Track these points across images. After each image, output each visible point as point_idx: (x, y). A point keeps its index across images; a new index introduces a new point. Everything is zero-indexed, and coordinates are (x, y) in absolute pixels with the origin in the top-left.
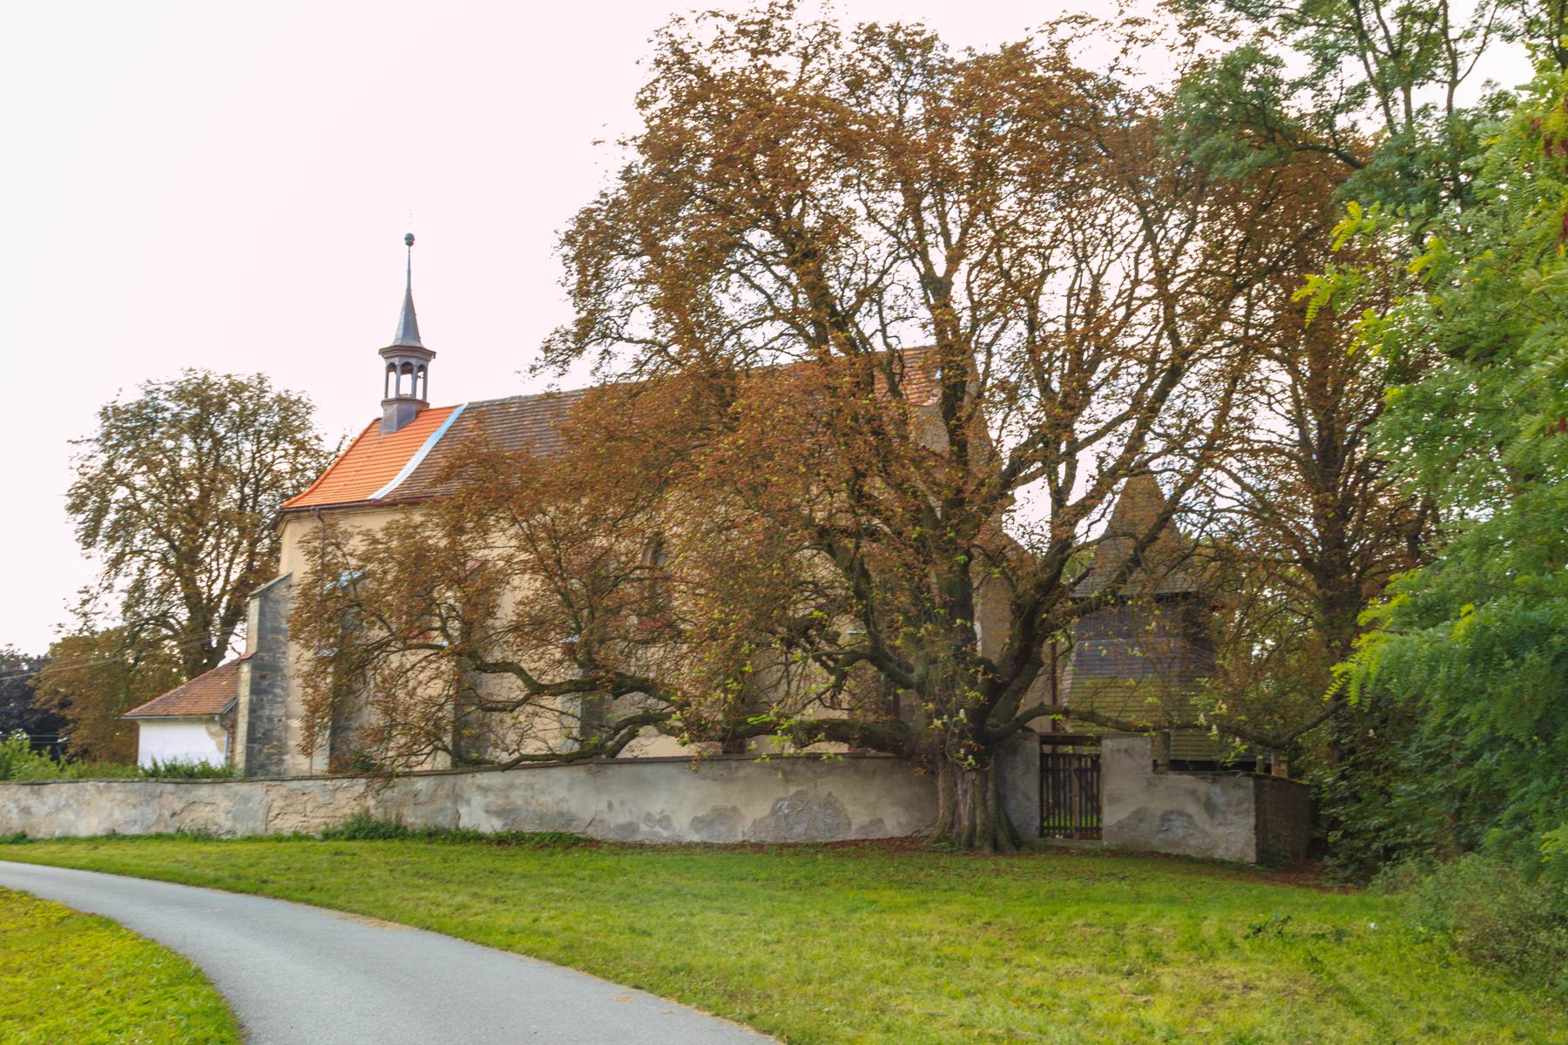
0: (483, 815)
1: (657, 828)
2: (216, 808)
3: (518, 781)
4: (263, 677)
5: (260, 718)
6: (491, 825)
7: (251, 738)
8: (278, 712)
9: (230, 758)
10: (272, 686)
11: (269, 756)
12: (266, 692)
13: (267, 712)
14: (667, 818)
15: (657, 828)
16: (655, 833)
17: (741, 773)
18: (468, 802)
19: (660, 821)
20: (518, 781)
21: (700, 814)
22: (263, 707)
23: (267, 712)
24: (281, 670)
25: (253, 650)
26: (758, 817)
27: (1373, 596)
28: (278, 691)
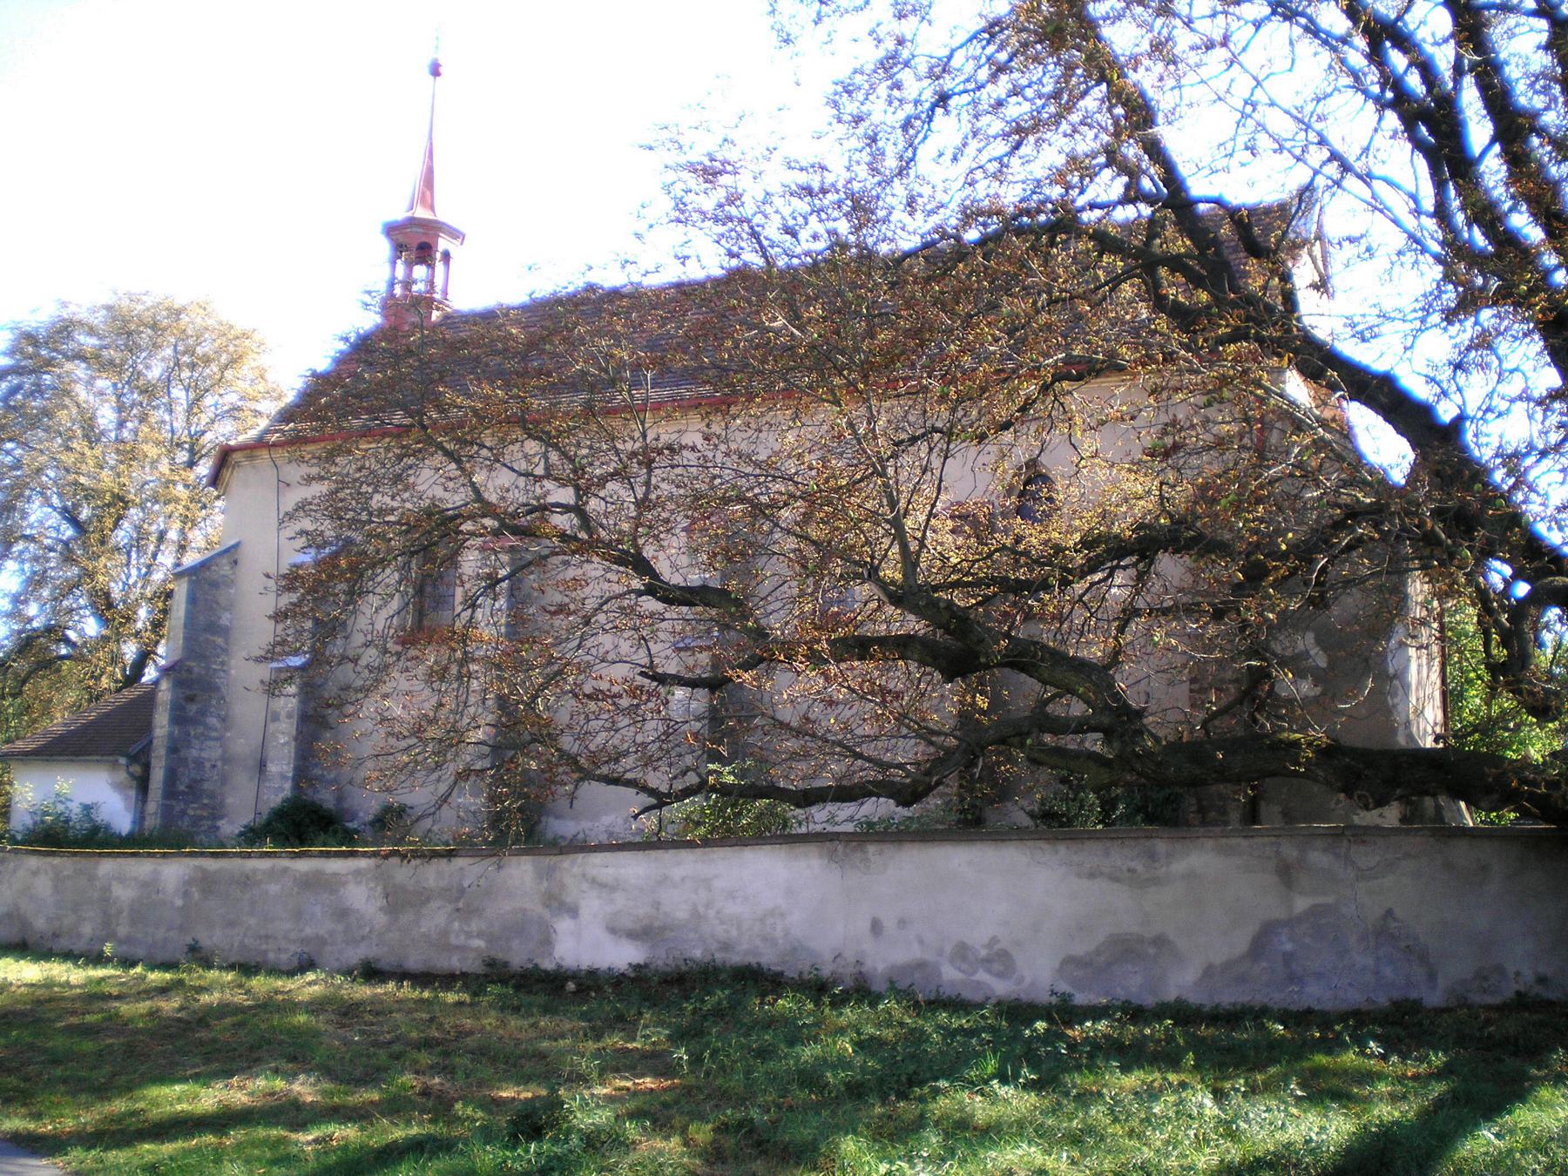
0: (606, 938)
1: (982, 976)
2: (124, 878)
3: (677, 873)
4: (191, 699)
5: (183, 761)
6: (621, 956)
7: (170, 792)
8: (212, 752)
9: (140, 817)
10: (203, 713)
11: (197, 820)
12: (194, 721)
13: (195, 753)
14: (1004, 956)
15: (982, 976)
16: (60, 798)
17: (1179, 866)
18: (574, 912)
19: (987, 961)
20: (677, 873)
21: (1079, 949)
22: (189, 746)
23: (195, 753)
24: (216, 689)
25: (176, 657)
26: (1218, 958)
27: (1111, 685)
28: (213, 721)
